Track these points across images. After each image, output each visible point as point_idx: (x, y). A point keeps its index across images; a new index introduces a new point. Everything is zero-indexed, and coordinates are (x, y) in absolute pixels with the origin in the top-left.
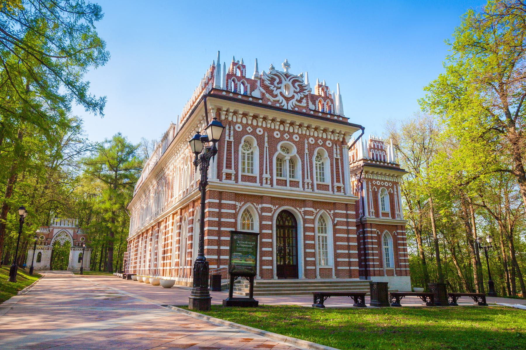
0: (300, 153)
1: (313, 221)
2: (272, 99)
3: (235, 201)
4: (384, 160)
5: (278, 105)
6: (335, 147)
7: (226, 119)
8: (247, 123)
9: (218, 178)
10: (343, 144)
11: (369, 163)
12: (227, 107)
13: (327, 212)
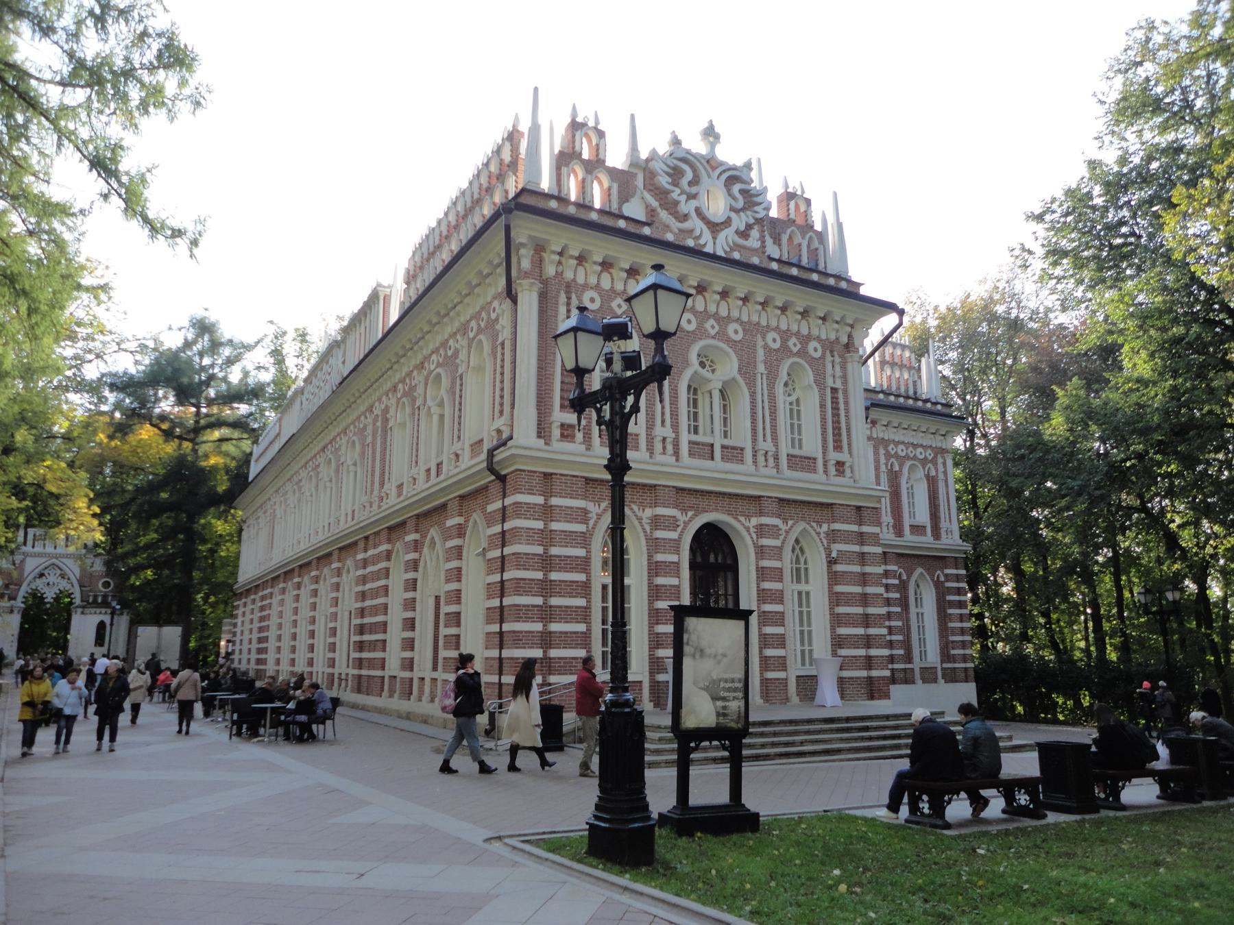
0: (745, 373)
1: (778, 552)
2: (675, 225)
3: (585, 498)
4: (915, 393)
5: (690, 243)
6: (829, 358)
7: (559, 274)
8: (612, 289)
9: (539, 437)
10: (849, 352)
11: (880, 400)
12: (563, 241)
13: (812, 527)
